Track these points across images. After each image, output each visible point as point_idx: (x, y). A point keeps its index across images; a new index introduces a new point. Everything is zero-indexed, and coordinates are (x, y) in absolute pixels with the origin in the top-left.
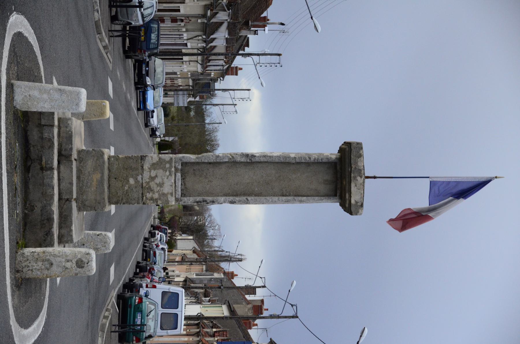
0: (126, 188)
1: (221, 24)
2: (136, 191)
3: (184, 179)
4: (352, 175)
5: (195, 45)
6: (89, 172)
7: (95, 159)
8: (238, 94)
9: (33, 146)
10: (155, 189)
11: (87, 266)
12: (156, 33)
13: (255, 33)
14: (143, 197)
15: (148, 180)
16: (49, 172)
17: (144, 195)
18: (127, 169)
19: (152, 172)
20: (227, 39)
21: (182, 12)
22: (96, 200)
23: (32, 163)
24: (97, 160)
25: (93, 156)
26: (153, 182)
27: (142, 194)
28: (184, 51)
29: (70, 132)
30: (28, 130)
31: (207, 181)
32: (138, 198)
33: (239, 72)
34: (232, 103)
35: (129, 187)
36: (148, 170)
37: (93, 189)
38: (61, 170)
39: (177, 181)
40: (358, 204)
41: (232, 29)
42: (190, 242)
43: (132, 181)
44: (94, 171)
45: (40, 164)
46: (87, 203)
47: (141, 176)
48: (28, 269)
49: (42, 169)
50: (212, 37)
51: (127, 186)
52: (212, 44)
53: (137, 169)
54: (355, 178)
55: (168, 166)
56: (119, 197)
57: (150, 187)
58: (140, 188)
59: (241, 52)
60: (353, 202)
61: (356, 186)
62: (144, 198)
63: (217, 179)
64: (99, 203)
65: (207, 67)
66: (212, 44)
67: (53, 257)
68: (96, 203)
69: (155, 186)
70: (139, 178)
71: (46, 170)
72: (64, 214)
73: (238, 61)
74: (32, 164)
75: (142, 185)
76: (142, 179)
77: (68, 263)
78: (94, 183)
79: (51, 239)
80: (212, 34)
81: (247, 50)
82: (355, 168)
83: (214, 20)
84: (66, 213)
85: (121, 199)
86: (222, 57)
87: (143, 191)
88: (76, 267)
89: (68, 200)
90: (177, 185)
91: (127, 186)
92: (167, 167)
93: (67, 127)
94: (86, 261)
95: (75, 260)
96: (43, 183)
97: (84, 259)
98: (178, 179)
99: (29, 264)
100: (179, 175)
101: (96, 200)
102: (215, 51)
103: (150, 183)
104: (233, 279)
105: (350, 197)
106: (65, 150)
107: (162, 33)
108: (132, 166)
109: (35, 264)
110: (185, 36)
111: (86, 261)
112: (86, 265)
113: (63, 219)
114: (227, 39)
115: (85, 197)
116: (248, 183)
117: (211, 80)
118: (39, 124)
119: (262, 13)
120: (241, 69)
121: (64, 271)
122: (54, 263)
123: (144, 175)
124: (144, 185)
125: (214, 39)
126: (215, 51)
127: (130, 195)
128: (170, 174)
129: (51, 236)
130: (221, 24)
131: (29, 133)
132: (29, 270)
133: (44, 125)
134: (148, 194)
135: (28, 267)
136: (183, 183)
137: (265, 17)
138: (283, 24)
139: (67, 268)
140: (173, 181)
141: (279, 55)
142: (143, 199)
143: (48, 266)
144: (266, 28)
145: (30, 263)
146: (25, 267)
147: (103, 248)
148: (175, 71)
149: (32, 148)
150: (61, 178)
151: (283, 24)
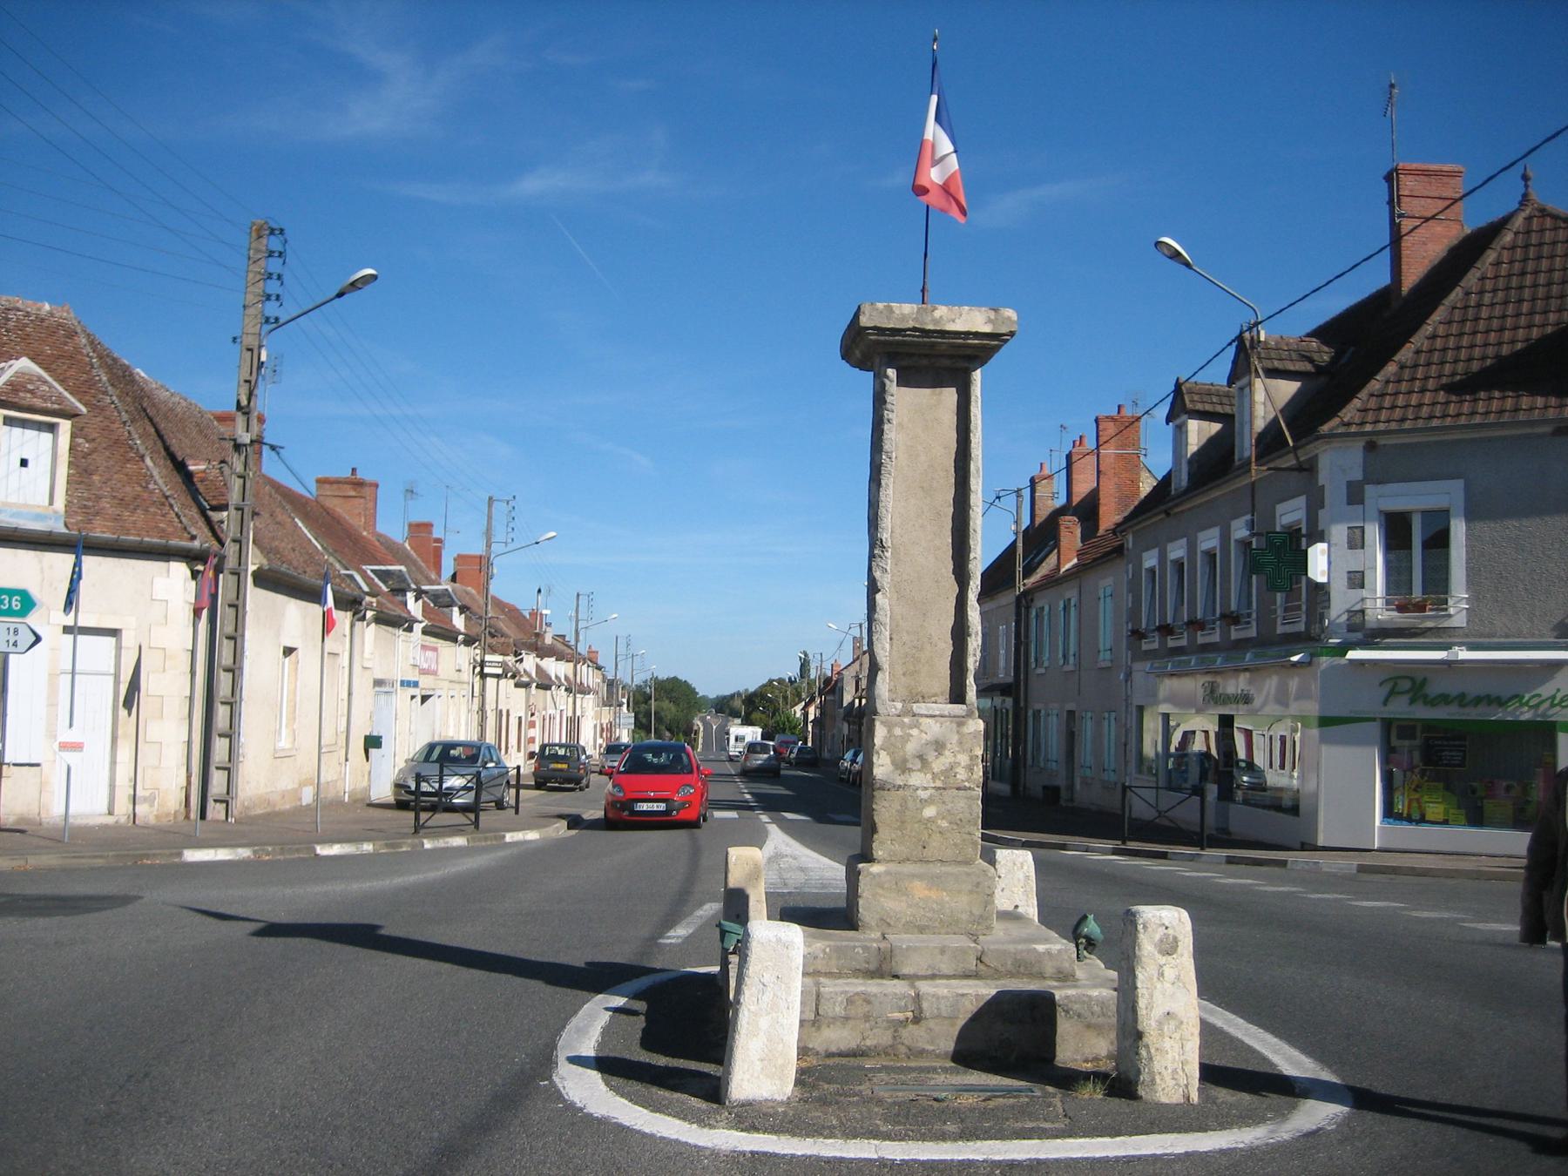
0: (945, 824)
1: (538, 666)
2: (953, 802)
3: (923, 697)
4: (931, 327)
5: (563, 701)
6: (910, 906)
7: (881, 891)
8: (622, 649)
9: (864, 1039)
10: (948, 761)
11: (1174, 928)
12: (557, 748)
13: (549, 625)
14: (965, 789)
15: (929, 776)
16: (925, 1005)
17: (962, 785)
18: (903, 822)
19: (911, 766)
20: (557, 660)
21: (522, 714)
22: (971, 892)
23: (903, 1044)
24: (883, 888)
25: (873, 895)
26: (934, 765)
27: (958, 789)
28: (570, 714)
29: (828, 950)
30: (826, 1051)
31: (928, 647)
32: (968, 798)
33: (593, 649)
34: (1386, 254)
35: (943, 818)
36: (907, 775)
37: (947, 899)
38: (912, 972)
39: (931, 713)
40: (993, 317)
41: (543, 652)
42: (130, 780)
43: (930, 812)
44: (908, 896)
45: (903, 1023)
46: (977, 911)
47: (919, 792)
48: (1181, 1073)
49: (917, 1020)
50: (553, 678)
51: (939, 821)
52: (563, 680)
53: (904, 800)
54: (936, 321)
55: (898, 731)
56: (964, 840)
57: (942, 772)
58: (945, 793)
59: (573, 643)
60: (987, 329)
61: (953, 321)
62: (966, 784)
63: (925, 624)
64: (978, 884)
65: (588, 686)
66: (563, 680)
67: (1151, 1010)
68: (977, 892)
69: (942, 759)
70: (923, 794)
71: (921, 1010)
72: (1009, 967)
73: (582, 649)
74: (906, 1042)
75: (939, 788)
76: (926, 789)
77: (1166, 974)
78: (933, 894)
79: (1075, 1002)
80: (551, 679)
81: (571, 638)
82: (915, 320)
83: (534, 675)
84: (1009, 963)
85: (968, 837)
86: (579, 666)
87: (951, 788)
88: (1174, 956)
89: (979, 959)
90: (938, 713)
91: (939, 821)
92: (900, 733)
93: (816, 958)
94: (1162, 930)
95: (1158, 956)
96: (950, 1018)
97: (1157, 937)
98: (928, 709)
99: (1170, 1071)
100: (919, 708)
101: (971, 892)
102: (571, 676)
103: (935, 770)
104: (697, 693)
105: (977, 335)
106: (868, 963)
107: (557, 741)
108: (897, 811)
109: (1170, 1056)
110: (551, 711)
111: (1162, 930)
112: (1170, 931)
113: (1022, 969)
114: (557, 660)
115: (964, 917)
116: (936, 558)
117: (604, 682)
118: (813, 1025)
119: (525, 617)
120: (590, 647)
121: (1184, 983)
122: (1167, 1009)
123: (918, 783)
124: (939, 784)
125: (557, 677)
126: (571, 676)
127: (961, 816)
128: (917, 726)
129: (1071, 1001)
130: (538, 666)
131: (833, 1049)
132: (1183, 1070)
133: (817, 1013)
134: (958, 776)
135: (1175, 1071)
136: (933, 699)
137: (530, 614)
138: (539, 591)
139: (1178, 978)
140: (928, 720)
141: (578, 595)
142: (970, 788)
143: (1173, 1023)
144: (544, 612)
145: (1166, 1068)
146: (1176, 1079)
147: (1025, 868)
148: (592, 726)
149: (868, 1043)
150: (929, 972)
151: (539, 591)
